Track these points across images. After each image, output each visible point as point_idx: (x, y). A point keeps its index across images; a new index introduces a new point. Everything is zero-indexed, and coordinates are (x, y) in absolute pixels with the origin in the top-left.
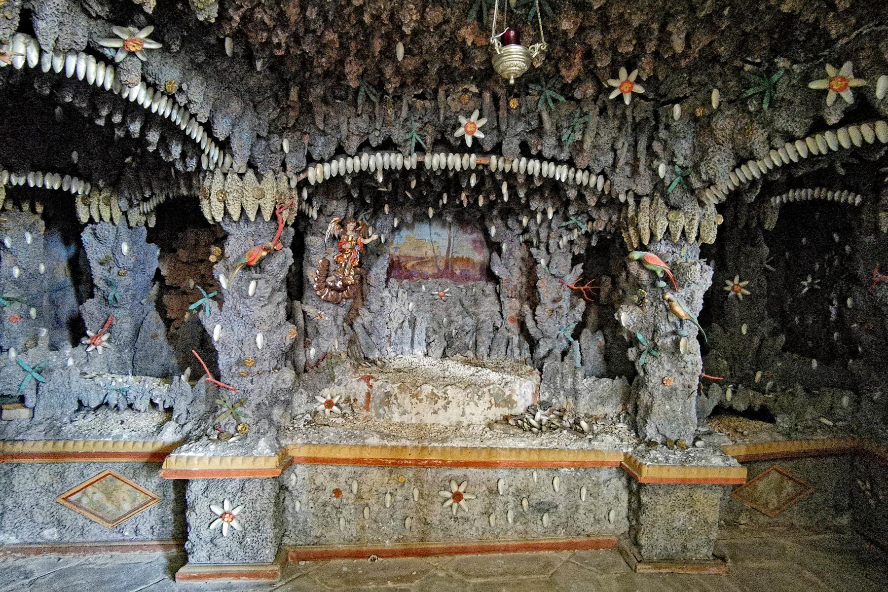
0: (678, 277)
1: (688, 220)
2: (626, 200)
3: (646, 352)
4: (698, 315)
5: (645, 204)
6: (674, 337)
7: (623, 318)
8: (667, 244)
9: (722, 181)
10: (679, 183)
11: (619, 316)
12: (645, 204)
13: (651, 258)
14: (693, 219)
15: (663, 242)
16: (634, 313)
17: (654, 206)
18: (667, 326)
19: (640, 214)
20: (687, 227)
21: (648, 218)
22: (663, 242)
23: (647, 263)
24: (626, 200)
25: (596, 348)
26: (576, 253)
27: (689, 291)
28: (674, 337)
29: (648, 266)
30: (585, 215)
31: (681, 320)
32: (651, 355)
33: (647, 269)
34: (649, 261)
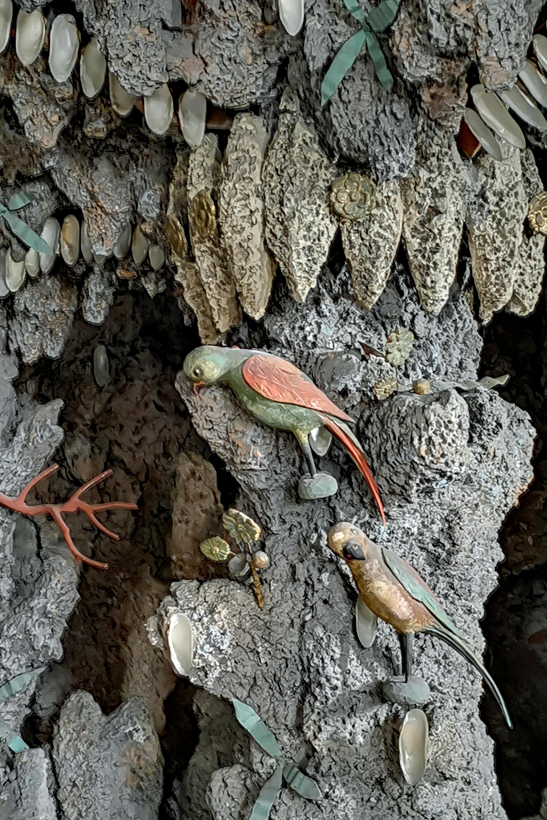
0: (382, 456)
1: (416, 216)
2: (176, 126)
3: (277, 781)
4: (480, 611)
5: (246, 142)
6: (383, 711)
7: (173, 637)
8: (344, 317)
9: (503, 51)
10: (365, 58)
11: (162, 632)
12: (246, 142)
13: (268, 370)
14: (436, 211)
15: (327, 305)
16: (223, 611)
17: (277, 154)
18: (354, 666)
19: (227, 186)
20: (414, 243)
21: (255, 203)
22: (327, 305)
23: (256, 396)
24: (176, 126)
25: (123, 773)
26: (31, 357)
27: (438, 513)
28: (383, 711)
29: (258, 409)
30: (40, 189)
31: (402, 637)
32: (294, 794)
33: (261, 424)
34: (263, 388)
